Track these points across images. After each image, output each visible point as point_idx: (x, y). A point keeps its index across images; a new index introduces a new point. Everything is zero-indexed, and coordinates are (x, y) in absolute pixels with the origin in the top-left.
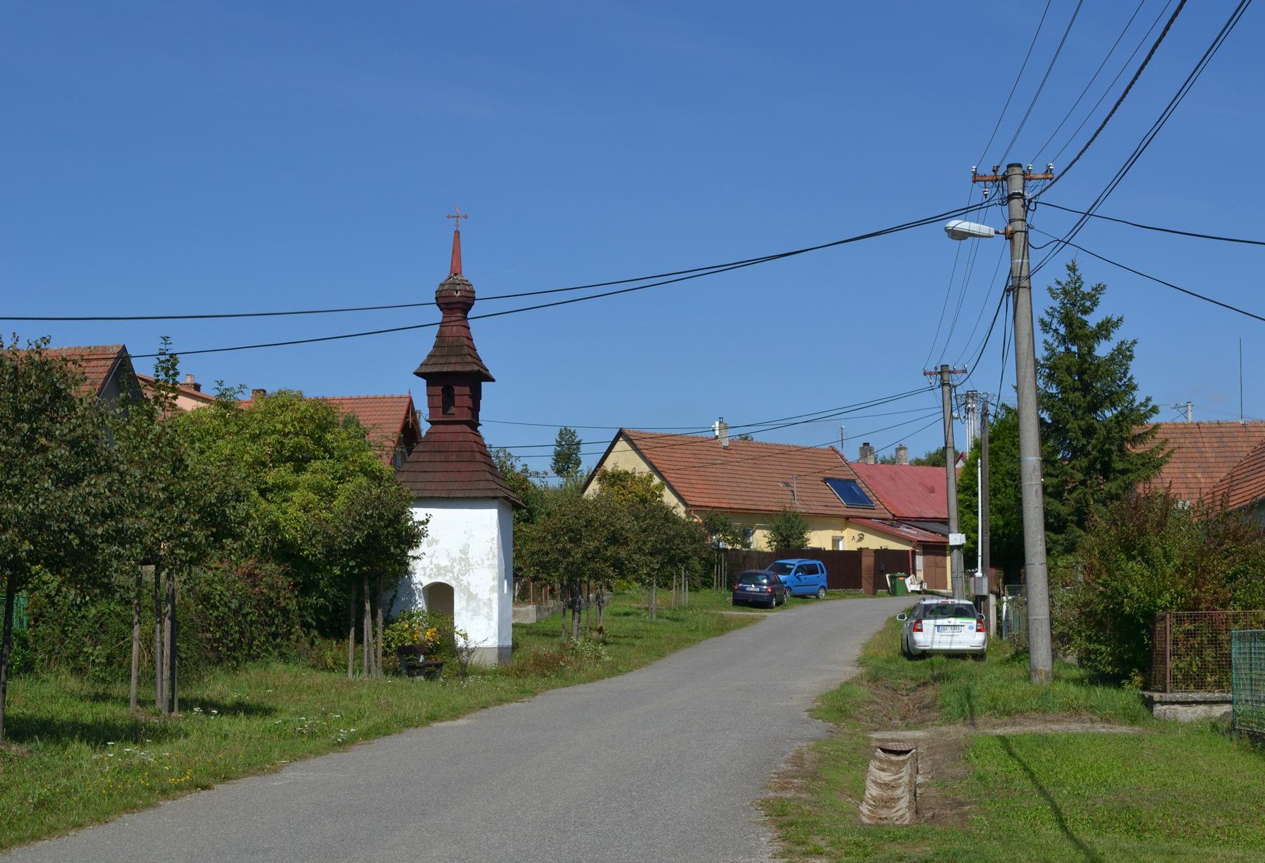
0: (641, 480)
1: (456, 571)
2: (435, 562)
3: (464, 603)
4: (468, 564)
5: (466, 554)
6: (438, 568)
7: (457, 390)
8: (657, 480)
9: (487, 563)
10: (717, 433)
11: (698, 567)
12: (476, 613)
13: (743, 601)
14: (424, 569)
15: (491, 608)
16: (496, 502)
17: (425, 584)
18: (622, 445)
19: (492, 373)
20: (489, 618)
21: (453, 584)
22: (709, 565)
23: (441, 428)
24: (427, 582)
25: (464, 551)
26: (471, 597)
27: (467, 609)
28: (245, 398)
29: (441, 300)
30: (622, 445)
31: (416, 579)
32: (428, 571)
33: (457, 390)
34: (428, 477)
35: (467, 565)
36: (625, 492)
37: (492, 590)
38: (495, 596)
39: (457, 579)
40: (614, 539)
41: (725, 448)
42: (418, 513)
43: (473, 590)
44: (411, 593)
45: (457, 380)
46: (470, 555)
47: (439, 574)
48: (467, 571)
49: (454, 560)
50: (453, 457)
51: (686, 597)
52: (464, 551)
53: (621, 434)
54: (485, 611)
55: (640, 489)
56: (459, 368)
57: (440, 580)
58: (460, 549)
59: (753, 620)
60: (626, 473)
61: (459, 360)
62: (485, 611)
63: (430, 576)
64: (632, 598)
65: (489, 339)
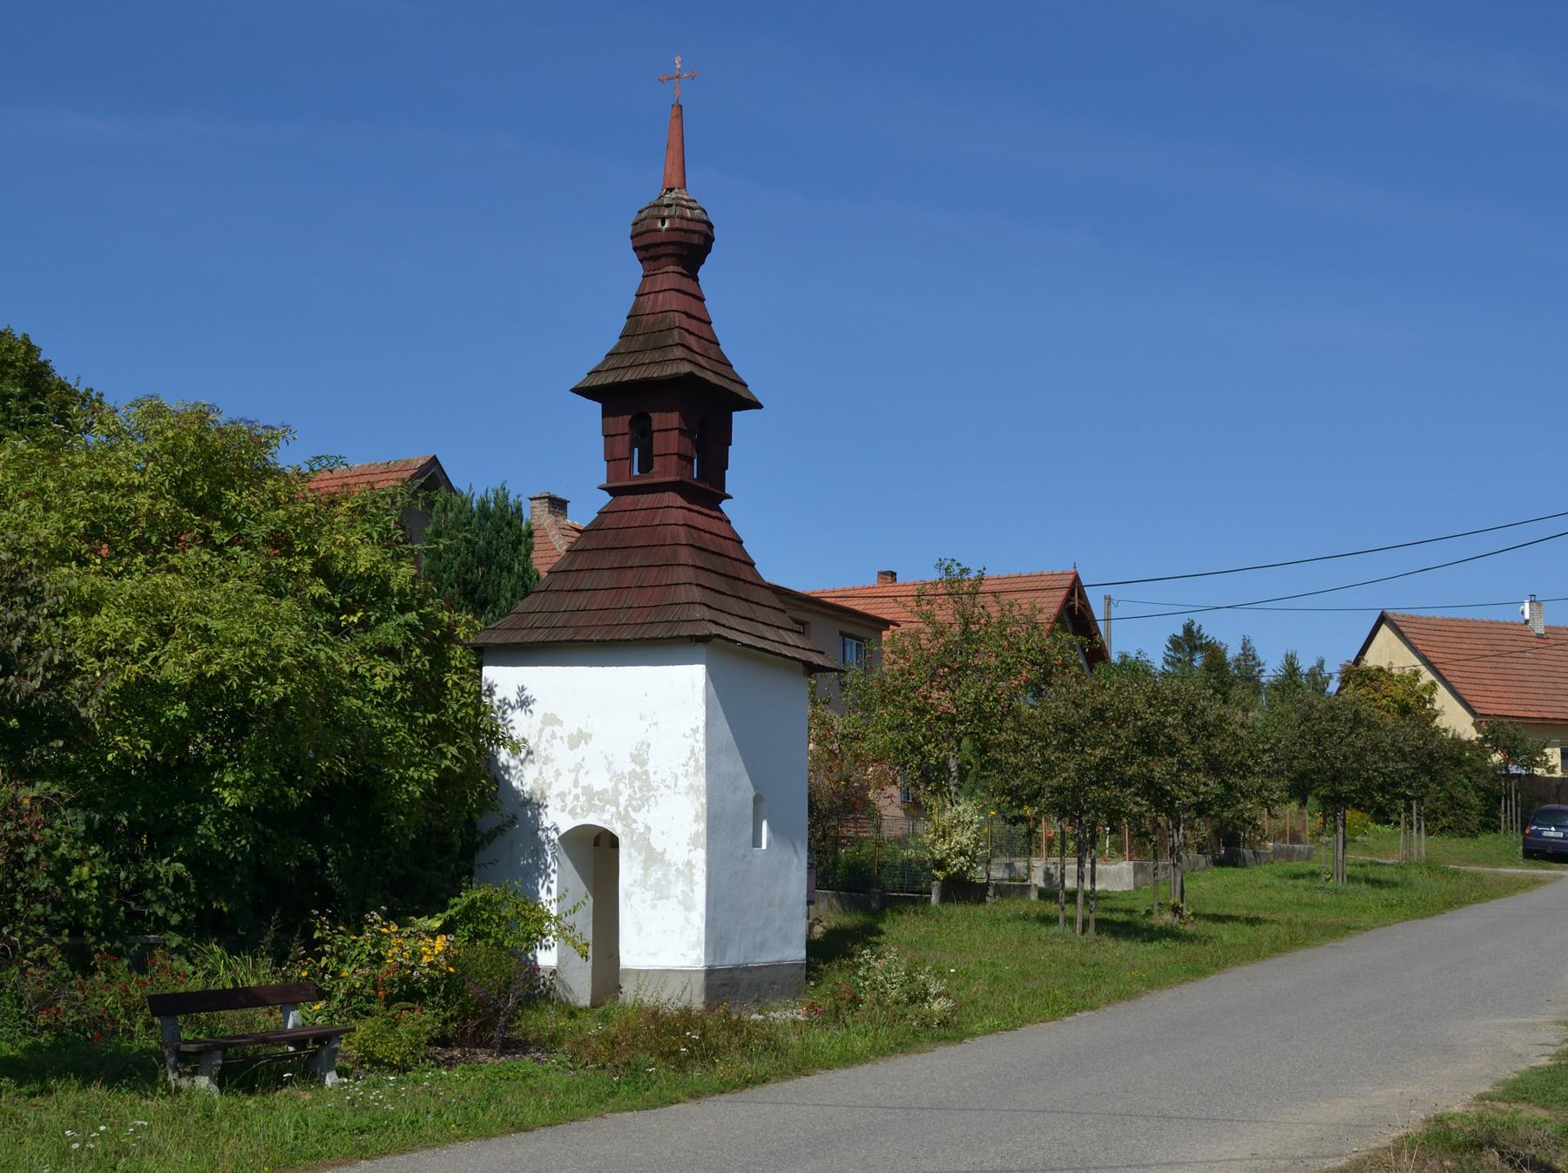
0: (1401, 679)
1: (623, 800)
2: (583, 782)
3: (638, 872)
4: (647, 786)
5: (643, 763)
6: (589, 793)
7: (658, 420)
8: (1427, 677)
9: (684, 783)
10: (1527, 616)
11: (1475, 801)
12: (661, 894)
13: (1538, 852)
14: (562, 796)
15: (691, 883)
16: (702, 649)
17: (563, 830)
18: (1385, 632)
19: (756, 391)
20: (688, 907)
21: (617, 829)
22: (1492, 800)
23: (627, 501)
24: (566, 824)
25: (639, 758)
26: (653, 858)
27: (643, 884)
28: (1137, 636)
29: (645, 240)
30: (1385, 632)
31: (546, 821)
32: (569, 799)
33: (658, 420)
34: (579, 601)
35: (643, 784)
36: (1377, 696)
37: (693, 842)
38: (700, 856)
39: (624, 818)
40: (1148, 743)
41: (1539, 636)
42: (502, 679)
43: (658, 843)
44: (538, 850)
45: (673, 409)
46: (650, 767)
47: (591, 808)
48: (645, 801)
49: (618, 778)
50: (636, 559)
51: (1422, 844)
52: (639, 758)
53: (1382, 619)
54: (678, 889)
55: (1398, 692)
56: (654, 372)
57: (592, 819)
58: (617, 750)
59: (1537, 882)
60: (1380, 670)
61: (656, 356)
62: (678, 889)
63: (573, 812)
64: (1365, 847)
65: (741, 308)
